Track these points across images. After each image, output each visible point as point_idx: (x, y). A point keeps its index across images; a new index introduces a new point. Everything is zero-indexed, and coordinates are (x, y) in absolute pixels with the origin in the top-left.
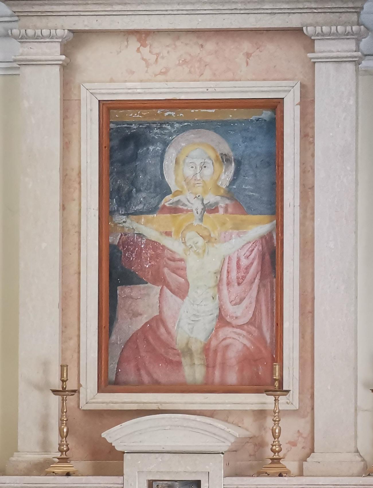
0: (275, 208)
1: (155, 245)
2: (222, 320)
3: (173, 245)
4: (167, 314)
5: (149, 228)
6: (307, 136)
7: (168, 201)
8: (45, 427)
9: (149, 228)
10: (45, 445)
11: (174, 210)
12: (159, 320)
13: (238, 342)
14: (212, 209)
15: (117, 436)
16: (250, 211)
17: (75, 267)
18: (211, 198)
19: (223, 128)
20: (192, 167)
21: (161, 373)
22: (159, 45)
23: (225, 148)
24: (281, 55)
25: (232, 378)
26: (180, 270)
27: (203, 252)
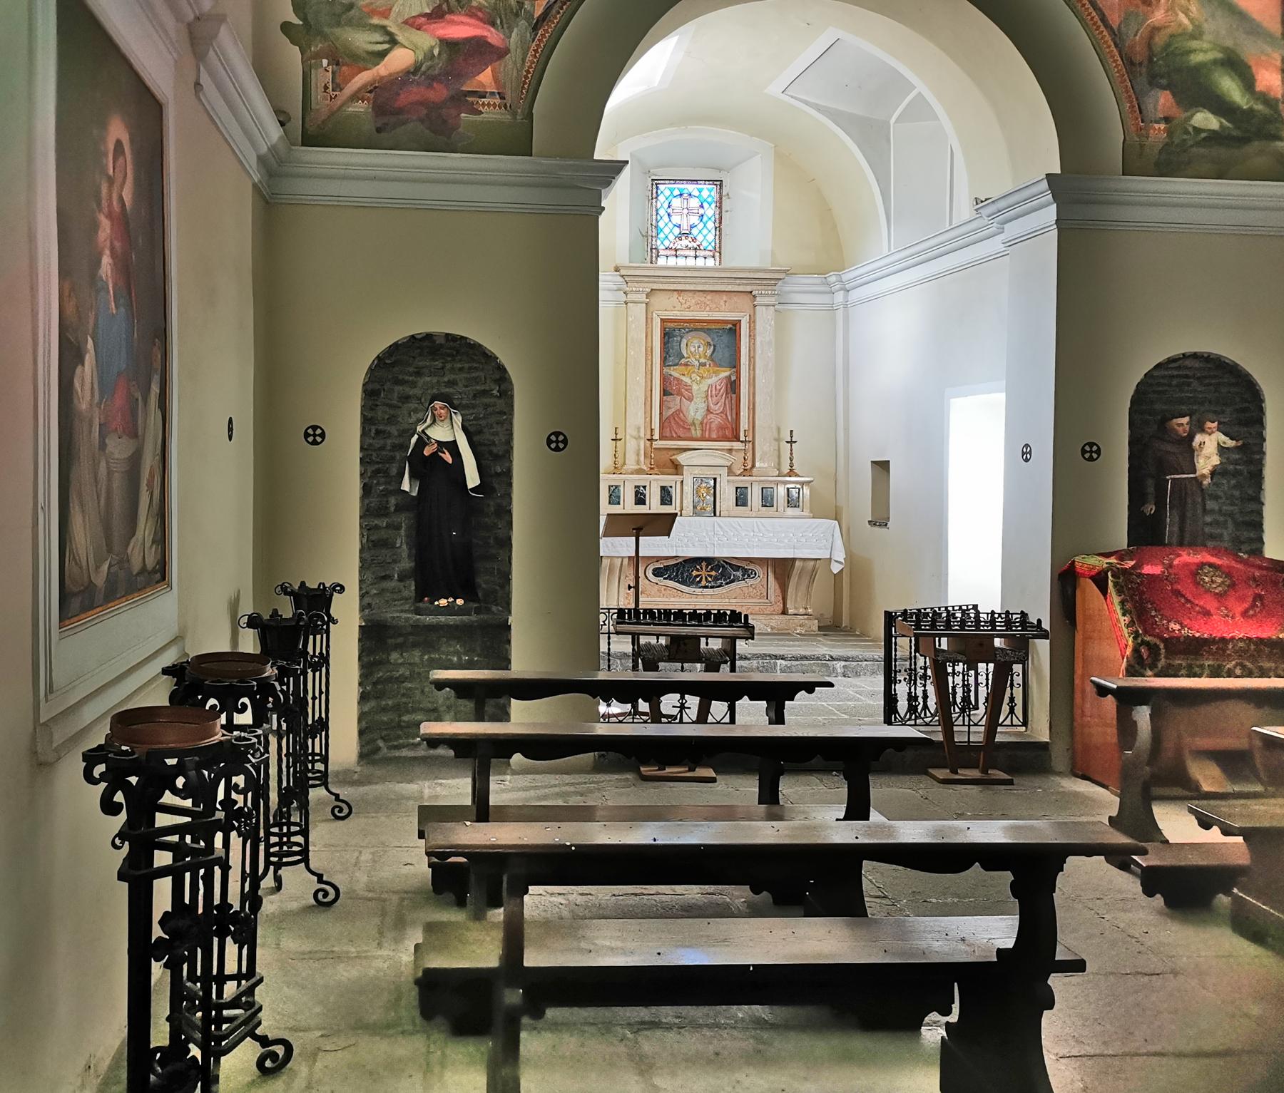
0: (735, 364)
1: (678, 379)
2: (709, 411)
3: (686, 379)
4: (684, 409)
5: (674, 372)
6: (752, 336)
7: (683, 361)
8: (638, 455)
9: (674, 372)
10: (638, 462)
11: (686, 365)
12: (680, 410)
13: (717, 420)
14: (704, 365)
15: (682, 458)
16: (720, 366)
17: (87, 372)
18: (702, 360)
19: (708, 331)
20: (694, 347)
21: (681, 432)
22: (686, 296)
23: (709, 340)
24: (744, 301)
25: (714, 436)
26: (689, 389)
27: (702, 385)
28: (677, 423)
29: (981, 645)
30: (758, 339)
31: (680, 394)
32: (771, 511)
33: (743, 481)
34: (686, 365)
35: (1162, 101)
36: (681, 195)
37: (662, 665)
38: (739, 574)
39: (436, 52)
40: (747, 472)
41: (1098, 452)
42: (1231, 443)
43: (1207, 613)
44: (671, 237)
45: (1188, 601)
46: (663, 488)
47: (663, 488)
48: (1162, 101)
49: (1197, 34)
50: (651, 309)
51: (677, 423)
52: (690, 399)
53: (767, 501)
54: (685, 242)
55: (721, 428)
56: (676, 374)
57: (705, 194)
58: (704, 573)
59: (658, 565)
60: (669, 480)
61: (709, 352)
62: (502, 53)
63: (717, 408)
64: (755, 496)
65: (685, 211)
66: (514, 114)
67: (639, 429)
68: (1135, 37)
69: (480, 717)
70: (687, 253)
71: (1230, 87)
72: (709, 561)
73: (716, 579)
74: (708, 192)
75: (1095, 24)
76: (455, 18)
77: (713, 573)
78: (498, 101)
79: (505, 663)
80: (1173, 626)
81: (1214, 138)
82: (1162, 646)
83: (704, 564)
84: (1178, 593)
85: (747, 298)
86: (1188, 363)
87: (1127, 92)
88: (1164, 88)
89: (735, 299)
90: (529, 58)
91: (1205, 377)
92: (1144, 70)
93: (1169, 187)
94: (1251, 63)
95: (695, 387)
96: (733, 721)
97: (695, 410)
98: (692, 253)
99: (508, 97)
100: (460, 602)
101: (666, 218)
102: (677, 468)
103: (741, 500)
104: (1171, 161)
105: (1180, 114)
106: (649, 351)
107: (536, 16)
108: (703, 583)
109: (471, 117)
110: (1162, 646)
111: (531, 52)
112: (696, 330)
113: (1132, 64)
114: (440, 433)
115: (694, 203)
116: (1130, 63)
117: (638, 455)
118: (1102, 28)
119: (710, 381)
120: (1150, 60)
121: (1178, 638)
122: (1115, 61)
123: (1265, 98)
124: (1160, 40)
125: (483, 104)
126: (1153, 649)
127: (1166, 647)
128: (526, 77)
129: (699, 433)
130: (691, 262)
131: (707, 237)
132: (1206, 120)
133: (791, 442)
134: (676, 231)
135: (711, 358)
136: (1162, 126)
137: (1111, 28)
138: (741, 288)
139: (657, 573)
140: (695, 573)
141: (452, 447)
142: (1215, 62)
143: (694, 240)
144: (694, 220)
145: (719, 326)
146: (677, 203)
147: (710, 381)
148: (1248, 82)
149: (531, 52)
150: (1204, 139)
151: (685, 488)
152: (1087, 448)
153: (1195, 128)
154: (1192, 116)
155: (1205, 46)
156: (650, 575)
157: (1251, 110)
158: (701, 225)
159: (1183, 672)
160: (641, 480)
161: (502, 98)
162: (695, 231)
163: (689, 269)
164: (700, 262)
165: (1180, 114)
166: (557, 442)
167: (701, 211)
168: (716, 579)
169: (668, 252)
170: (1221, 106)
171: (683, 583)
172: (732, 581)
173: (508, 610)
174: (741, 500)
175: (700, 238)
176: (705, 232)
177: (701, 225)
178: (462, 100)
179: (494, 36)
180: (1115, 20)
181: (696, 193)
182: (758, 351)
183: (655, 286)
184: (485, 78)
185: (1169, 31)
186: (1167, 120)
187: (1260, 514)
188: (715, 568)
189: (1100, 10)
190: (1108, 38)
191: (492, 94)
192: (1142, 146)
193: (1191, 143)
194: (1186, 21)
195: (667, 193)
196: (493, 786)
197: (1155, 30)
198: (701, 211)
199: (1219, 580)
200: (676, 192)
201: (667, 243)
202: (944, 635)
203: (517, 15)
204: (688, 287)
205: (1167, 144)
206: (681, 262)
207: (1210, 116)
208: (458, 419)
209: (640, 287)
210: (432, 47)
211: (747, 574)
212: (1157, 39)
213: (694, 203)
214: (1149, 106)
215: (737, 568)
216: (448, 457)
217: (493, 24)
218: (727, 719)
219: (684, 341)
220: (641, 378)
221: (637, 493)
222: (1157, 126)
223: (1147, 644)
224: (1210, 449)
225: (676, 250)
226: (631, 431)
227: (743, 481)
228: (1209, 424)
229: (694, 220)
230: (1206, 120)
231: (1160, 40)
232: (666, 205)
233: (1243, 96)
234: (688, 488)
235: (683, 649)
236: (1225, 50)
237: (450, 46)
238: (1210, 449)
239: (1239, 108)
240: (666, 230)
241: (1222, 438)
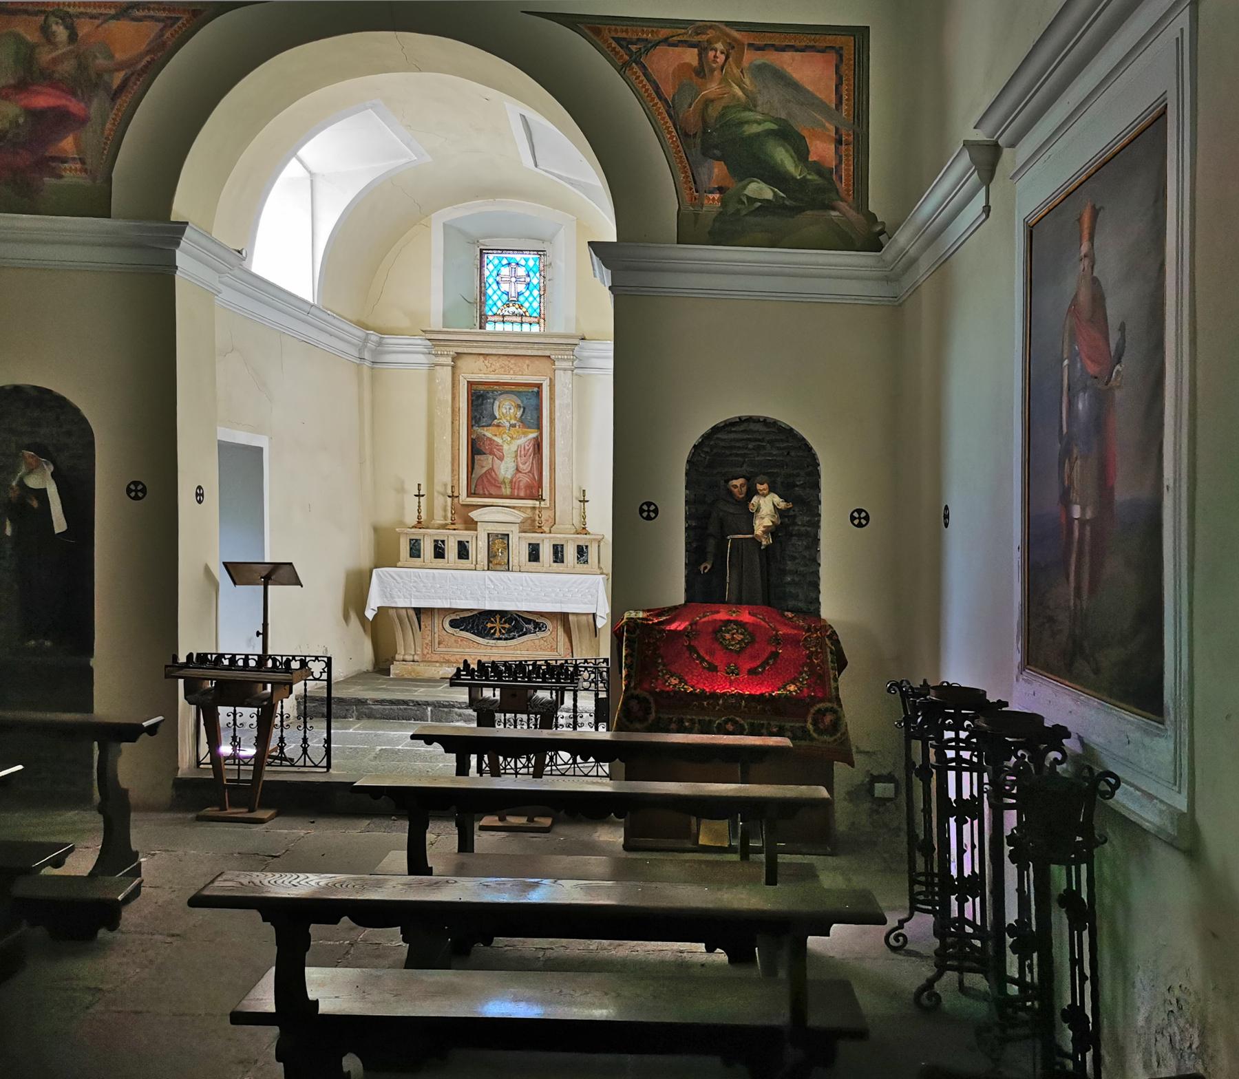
0: (539, 427)
1: (490, 439)
6: (552, 399)
7: (496, 422)
8: (445, 510)
10: (445, 518)
11: (498, 426)
12: (492, 469)
13: (524, 479)
14: (514, 426)
15: (474, 515)
18: (513, 422)
19: (518, 394)
20: (506, 409)
22: (491, 359)
23: (519, 402)
25: (522, 494)
26: (500, 450)
27: (510, 447)
28: (489, 481)
29: (514, 695)
30: (557, 402)
31: (492, 453)
32: (417, 561)
33: (534, 537)
34: (498, 426)
35: (717, 171)
36: (509, 264)
37: (499, 716)
38: (531, 627)
39: (21, 120)
40: (538, 529)
41: (656, 511)
42: (782, 505)
43: (713, 668)
44: (499, 304)
45: (699, 657)
46: (460, 543)
47: (460, 543)
48: (716, 170)
49: (750, 105)
50: (458, 371)
51: (489, 481)
52: (501, 459)
53: (439, 553)
54: (512, 309)
55: (529, 487)
56: (489, 435)
57: (531, 263)
58: (498, 626)
59: (454, 617)
60: (465, 535)
61: (519, 414)
62: (83, 121)
63: (525, 468)
64: (546, 552)
65: (513, 280)
66: (94, 179)
67: (445, 485)
68: (689, 112)
69: (744, 781)
70: (514, 319)
71: (783, 157)
72: (502, 613)
73: (509, 631)
74: (532, 260)
75: (649, 95)
76: (39, 88)
77: (507, 626)
78: (79, 166)
79: (88, 706)
80: (674, 681)
81: (766, 207)
82: (651, 700)
83: (498, 617)
84: (691, 649)
85: (547, 363)
86: (753, 426)
87: (681, 162)
88: (718, 159)
89: (537, 362)
90: (108, 126)
91: (776, 440)
92: (698, 141)
93: (697, 254)
94: (805, 133)
95: (505, 447)
96: (329, 766)
97: (505, 470)
98: (519, 319)
99: (89, 161)
100: (48, 643)
101: (495, 286)
102: (471, 525)
103: (534, 554)
104: (724, 231)
105: (732, 184)
106: (455, 412)
107: (115, 87)
108: (497, 635)
109: (53, 181)
110: (651, 700)
111: (110, 121)
112: (507, 392)
113: (686, 135)
114: (33, 482)
115: (521, 272)
116: (685, 135)
117: (445, 510)
118: (656, 100)
119: (519, 442)
120: (705, 132)
121: (675, 692)
122: (670, 133)
123: (818, 168)
124: (713, 112)
125: (65, 169)
126: (643, 701)
127: (656, 701)
128: (106, 144)
129: (508, 492)
130: (517, 328)
131: (531, 303)
132: (759, 190)
133: (419, 496)
134: (505, 298)
135: (521, 420)
136: (717, 196)
137: (666, 101)
138: (540, 353)
139: (454, 624)
140: (489, 625)
141: (42, 494)
142: (769, 133)
143: (521, 307)
144: (521, 288)
145: (525, 389)
146: (505, 271)
147: (519, 442)
148: (801, 153)
149: (110, 121)
150: (758, 209)
151: (480, 543)
152: (645, 507)
153: (749, 198)
154: (744, 188)
155: (759, 117)
156: (447, 626)
157: (804, 179)
158: (527, 293)
159: (673, 726)
160: (441, 534)
161: (82, 161)
162: (521, 299)
163: (521, 334)
164: (526, 328)
165: (732, 184)
166: (136, 491)
167: (528, 280)
168: (509, 631)
169: (496, 318)
170: (775, 177)
171: (479, 634)
172: (525, 634)
173: (89, 651)
174: (534, 554)
175: (526, 305)
176: (531, 299)
177: (527, 293)
178: (49, 164)
179: (74, 106)
180: (668, 90)
181: (522, 262)
182: (557, 414)
183: (460, 350)
184: (67, 144)
185: (723, 103)
186: (721, 190)
187: (817, 574)
188: (509, 621)
189: (655, 81)
190: (662, 110)
191: (74, 159)
192: (697, 215)
193: (744, 213)
194: (740, 93)
195: (496, 262)
196: (430, 837)
197: (708, 102)
198: (528, 280)
199: (728, 636)
200: (505, 262)
201: (495, 310)
202: (498, 686)
203: (96, 85)
204: (494, 351)
205: (721, 213)
206: (508, 328)
207: (763, 185)
208: (50, 469)
209: (445, 350)
210: (17, 116)
211: (539, 627)
212: (710, 110)
213: (521, 272)
214: (703, 173)
215: (528, 621)
216: (35, 504)
217: (74, 94)
218: (324, 763)
219: (497, 403)
220: (447, 437)
221: (436, 547)
222: (711, 196)
223: (637, 697)
224: (766, 507)
225: (503, 316)
226: (438, 487)
227: (534, 537)
228: (759, 487)
229: (521, 288)
230: (759, 190)
231: (713, 112)
232: (495, 274)
233: (796, 166)
234: (483, 543)
235: (517, 701)
236: (776, 120)
237: (36, 115)
238: (766, 507)
239: (794, 178)
240: (495, 298)
241: (777, 499)
